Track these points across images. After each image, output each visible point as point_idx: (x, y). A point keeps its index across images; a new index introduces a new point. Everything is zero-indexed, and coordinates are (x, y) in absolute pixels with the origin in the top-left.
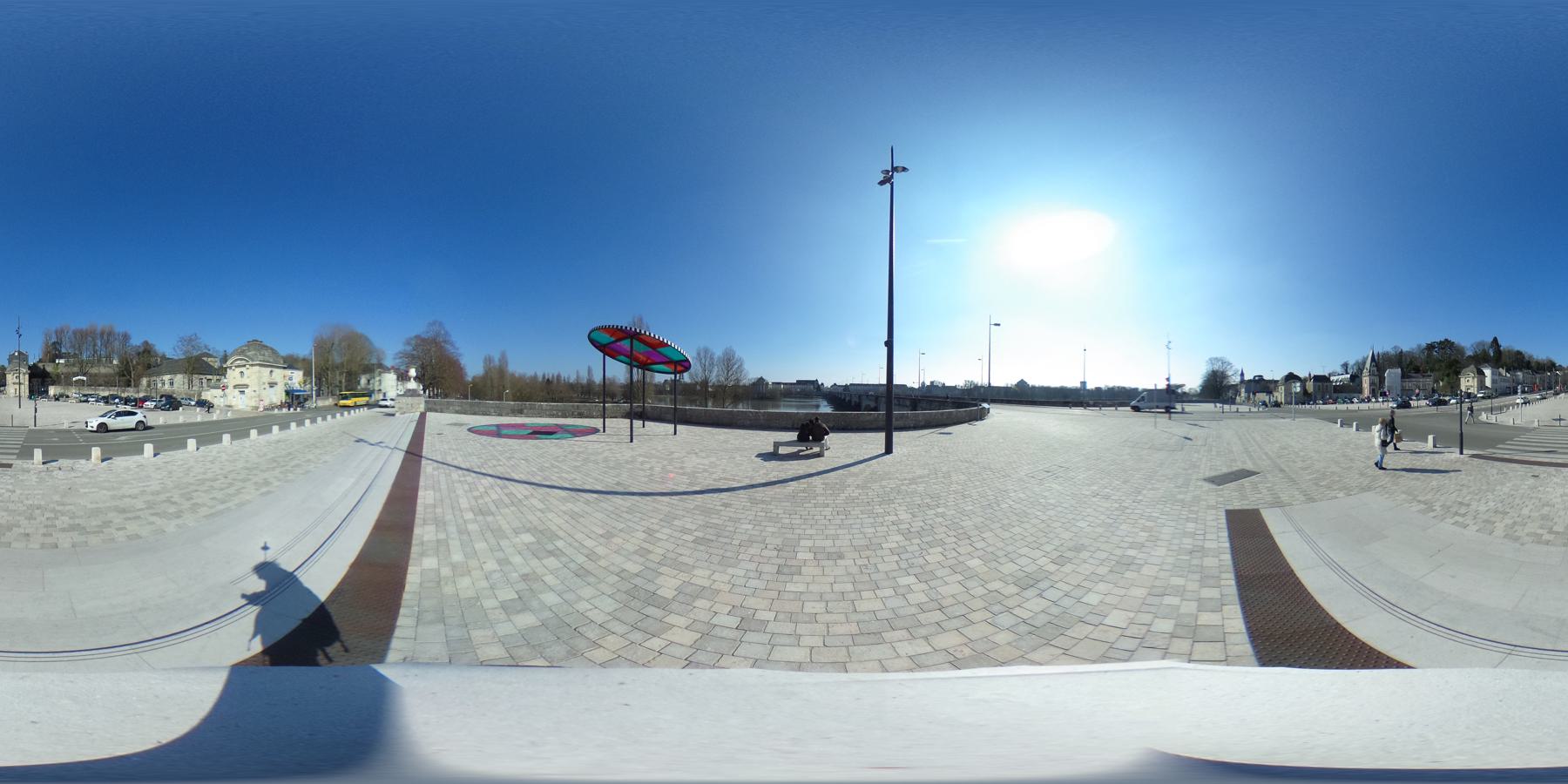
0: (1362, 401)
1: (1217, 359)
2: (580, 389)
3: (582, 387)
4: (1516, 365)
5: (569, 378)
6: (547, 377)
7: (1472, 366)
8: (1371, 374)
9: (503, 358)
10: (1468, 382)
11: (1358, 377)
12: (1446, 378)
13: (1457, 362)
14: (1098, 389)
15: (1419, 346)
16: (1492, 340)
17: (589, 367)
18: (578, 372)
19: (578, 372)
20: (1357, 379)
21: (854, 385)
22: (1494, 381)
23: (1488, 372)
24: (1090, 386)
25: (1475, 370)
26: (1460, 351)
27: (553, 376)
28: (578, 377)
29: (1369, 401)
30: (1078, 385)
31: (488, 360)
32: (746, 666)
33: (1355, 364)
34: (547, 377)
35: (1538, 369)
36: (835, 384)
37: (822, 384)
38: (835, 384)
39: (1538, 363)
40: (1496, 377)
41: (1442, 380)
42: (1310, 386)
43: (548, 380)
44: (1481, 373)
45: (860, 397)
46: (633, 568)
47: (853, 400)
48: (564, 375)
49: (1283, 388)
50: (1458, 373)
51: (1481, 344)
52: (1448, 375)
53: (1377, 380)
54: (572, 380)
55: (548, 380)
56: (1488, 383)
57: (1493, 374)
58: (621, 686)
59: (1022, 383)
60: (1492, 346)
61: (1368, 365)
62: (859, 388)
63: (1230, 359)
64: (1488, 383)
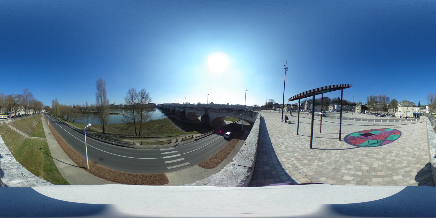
0: (305, 111)
1: (271, 100)
2: (84, 109)
3: (85, 108)
4: (344, 104)
5: (81, 106)
6: (74, 106)
7: (332, 104)
8: (307, 105)
9: (56, 99)
10: (330, 108)
11: (303, 105)
12: (325, 107)
13: (329, 103)
14: (232, 105)
15: (319, 98)
16: (338, 97)
17: (86, 102)
18: (83, 104)
19: (83, 104)
20: (303, 106)
21: (165, 104)
22: (337, 108)
23: (336, 106)
24: (230, 104)
25: (332, 105)
26: (330, 100)
27: (76, 105)
28: (83, 105)
29: (307, 111)
30: (226, 104)
31: (53, 101)
32: (232, 185)
33: (302, 102)
34: (74, 106)
35: (351, 105)
36: (159, 104)
37: (155, 104)
38: (159, 104)
39: (351, 104)
40: (338, 107)
41: (325, 107)
42: (292, 107)
43: (75, 106)
44: (334, 106)
45: (175, 107)
46: (244, 183)
47: (167, 108)
48: (79, 105)
49: (286, 107)
50: (328, 105)
51: (335, 98)
52: (326, 106)
53: (308, 106)
54: (82, 106)
55: (75, 106)
56: (336, 108)
57: (337, 106)
58: (41, 150)
59: (212, 103)
60: (338, 99)
61: (306, 102)
62: (166, 105)
63: (274, 100)
64: (336, 108)
